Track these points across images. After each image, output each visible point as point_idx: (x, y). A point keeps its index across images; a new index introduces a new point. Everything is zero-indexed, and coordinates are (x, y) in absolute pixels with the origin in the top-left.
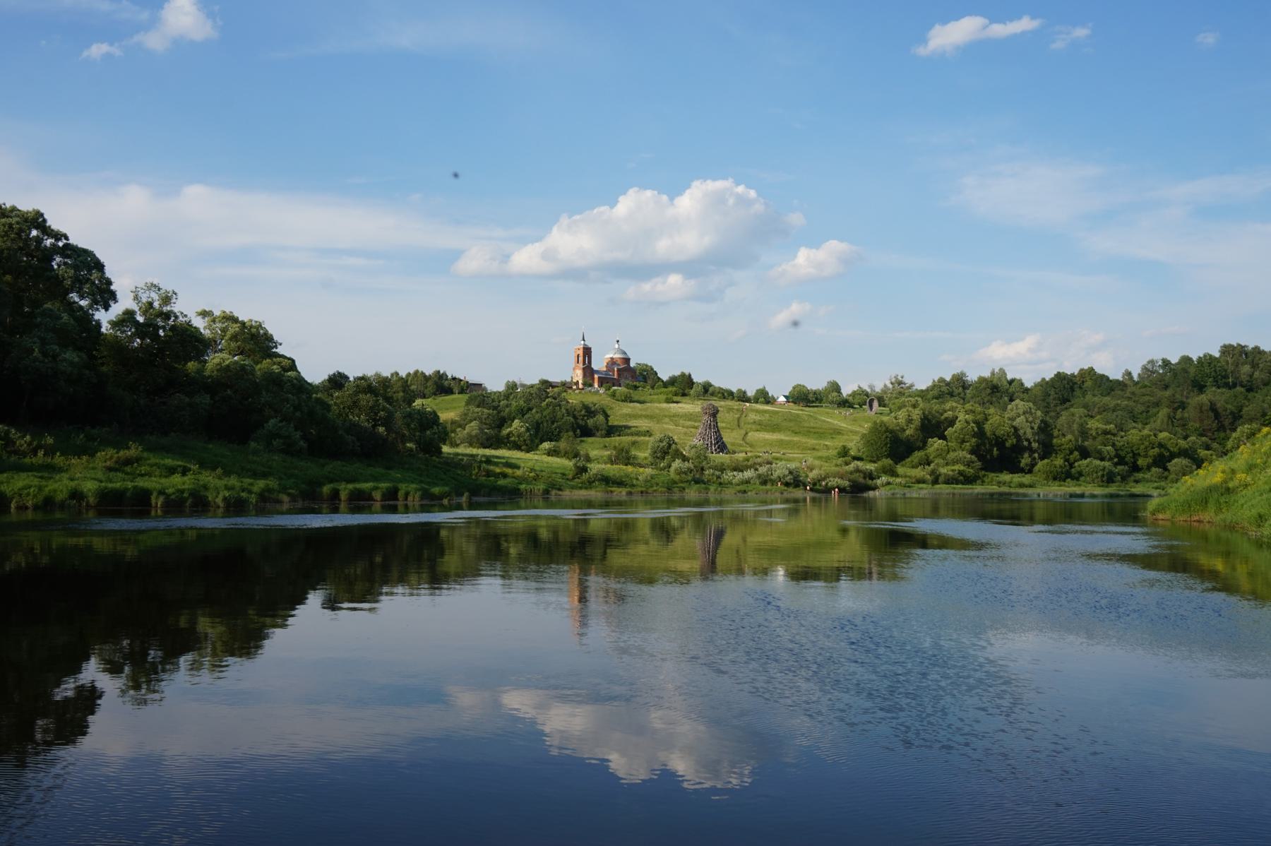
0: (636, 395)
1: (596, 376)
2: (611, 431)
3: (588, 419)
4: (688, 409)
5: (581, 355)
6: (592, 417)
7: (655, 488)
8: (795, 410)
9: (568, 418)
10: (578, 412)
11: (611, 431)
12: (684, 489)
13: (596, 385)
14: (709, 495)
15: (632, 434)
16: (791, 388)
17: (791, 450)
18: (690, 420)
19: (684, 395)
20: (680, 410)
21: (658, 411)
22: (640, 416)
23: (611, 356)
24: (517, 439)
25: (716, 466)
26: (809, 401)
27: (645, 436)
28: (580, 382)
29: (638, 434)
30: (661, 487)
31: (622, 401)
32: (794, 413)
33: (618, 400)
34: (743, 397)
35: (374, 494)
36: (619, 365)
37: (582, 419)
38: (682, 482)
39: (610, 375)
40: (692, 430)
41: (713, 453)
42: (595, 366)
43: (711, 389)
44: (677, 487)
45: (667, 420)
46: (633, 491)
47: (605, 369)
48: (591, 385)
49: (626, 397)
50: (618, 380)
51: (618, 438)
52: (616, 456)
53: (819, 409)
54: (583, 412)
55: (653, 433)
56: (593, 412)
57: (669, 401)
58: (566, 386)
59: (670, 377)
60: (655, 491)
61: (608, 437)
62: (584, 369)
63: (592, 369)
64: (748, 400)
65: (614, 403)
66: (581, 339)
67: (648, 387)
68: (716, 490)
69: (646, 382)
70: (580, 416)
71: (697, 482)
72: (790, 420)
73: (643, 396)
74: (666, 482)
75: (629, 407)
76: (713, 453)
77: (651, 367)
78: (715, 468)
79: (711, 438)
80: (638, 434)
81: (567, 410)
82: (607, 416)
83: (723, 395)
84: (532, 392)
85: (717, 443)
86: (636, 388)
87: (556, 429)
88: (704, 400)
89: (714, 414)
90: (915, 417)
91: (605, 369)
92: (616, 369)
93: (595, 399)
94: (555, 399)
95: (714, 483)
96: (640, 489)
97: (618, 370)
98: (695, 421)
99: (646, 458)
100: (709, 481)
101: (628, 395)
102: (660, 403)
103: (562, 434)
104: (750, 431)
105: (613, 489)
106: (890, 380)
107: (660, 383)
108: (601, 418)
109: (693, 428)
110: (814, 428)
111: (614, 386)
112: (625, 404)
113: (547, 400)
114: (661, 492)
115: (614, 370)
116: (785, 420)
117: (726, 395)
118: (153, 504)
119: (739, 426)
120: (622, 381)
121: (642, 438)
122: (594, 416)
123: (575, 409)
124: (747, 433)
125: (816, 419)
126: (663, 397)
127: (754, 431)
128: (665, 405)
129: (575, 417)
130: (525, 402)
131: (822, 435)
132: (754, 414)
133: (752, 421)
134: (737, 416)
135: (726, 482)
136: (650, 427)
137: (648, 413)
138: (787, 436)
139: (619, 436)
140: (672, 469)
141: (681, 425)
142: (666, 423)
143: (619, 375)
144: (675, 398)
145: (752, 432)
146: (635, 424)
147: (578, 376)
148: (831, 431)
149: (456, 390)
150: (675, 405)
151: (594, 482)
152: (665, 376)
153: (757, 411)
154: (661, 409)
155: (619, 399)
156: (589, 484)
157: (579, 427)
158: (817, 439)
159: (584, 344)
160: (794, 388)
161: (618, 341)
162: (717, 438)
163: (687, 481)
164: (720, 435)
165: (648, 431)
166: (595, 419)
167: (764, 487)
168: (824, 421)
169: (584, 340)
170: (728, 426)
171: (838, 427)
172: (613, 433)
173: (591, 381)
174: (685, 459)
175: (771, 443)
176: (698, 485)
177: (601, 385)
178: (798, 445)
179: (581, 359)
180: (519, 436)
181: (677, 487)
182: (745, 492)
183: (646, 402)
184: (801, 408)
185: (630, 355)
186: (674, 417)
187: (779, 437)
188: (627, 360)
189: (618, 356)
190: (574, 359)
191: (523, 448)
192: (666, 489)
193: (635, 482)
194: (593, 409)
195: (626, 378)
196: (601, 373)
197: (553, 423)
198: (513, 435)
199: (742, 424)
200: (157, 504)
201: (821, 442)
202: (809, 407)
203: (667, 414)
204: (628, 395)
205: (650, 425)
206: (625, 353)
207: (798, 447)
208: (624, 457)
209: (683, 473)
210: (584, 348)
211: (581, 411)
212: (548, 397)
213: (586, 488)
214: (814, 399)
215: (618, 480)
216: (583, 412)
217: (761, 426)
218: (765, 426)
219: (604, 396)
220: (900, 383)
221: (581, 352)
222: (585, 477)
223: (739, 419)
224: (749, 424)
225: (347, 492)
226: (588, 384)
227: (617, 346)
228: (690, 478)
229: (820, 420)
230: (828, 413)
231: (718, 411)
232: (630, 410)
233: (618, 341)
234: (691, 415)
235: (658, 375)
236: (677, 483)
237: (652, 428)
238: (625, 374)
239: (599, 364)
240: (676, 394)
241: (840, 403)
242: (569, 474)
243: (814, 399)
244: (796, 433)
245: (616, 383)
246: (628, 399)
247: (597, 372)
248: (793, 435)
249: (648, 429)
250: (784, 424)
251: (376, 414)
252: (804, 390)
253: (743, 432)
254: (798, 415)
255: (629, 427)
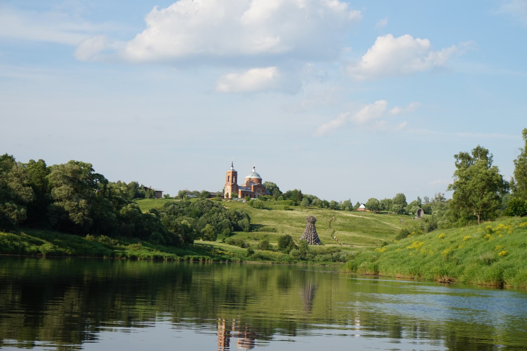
0: (266, 204)
1: (240, 190)
2: (252, 228)
3: (238, 220)
4: (298, 214)
5: (231, 176)
6: (240, 219)
7: (283, 262)
8: (370, 216)
9: (226, 219)
10: (232, 216)
11: (252, 228)
12: (296, 262)
13: (240, 196)
14: (308, 265)
15: (264, 230)
16: (368, 201)
17: (359, 243)
18: (299, 222)
19: (296, 205)
20: (294, 215)
21: (280, 216)
22: (269, 219)
23: (249, 177)
24: (208, 235)
25: (312, 252)
26: (379, 210)
27: (272, 232)
28: (230, 194)
29: (268, 230)
30: (286, 261)
31: (257, 208)
32: (366, 219)
33: (255, 208)
34: (335, 207)
35: (199, 259)
36: (254, 183)
37: (235, 220)
38: (296, 259)
39: (249, 190)
40: (301, 228)
41: (312, 244)
42: (239, 183)
43: (314, 201)
44: (293, 262)
45: (285, 221)
46: (274, 262)
47: (245, 186)
48: (237, 197)
49: (260, 205)
50: (254, 193)
51: (256, 233)
52: (261, 245)
53: (386, 215)
54: (235, 216)
55: (277, 230)
56: (241, 216)
57: (286, 209)
58: (221, 196)
59: (287, 192)
60: (283, 263)
61: (251, 232)
62: (232, 185)
63: (237, 185)
64: (338, 209)
65: (252, 209)
66: (231, 166)
67: (274, 199)
68: (311, 263)
69: (272, 195)
70: (233, 218)
71: (302, 259)
72: (363, 224)
73: (270, 205)
74: (288, 259)
75: (262, 212)
76: (312, 244)
77: (275, 184)
78: (312, 253)
79: (311, 235)
80: (268, 230)
81: (225, 214)
82: (249, 219)
83: (322, 205)
84: (204, 203)
85: (315, 238)
86: (266, 199)
87: (219, 227)
88: (309, 208)
89: (314, 221)
90: (425, 228)
91: (245, 186)
92: (252, 186)
93: (240, 206)
94: (217, 207)
95: (310, 260)
96: (277, 262)
97: (254, 187)
98: (303, 223)
99: (276, 247)
100: (308, 259)
101: (261, 205)
102: (281, 210)
103: (223, 229)
104: (336, 231)
105: (265, 261)
106: (435, 196)
107: (281, 197)
108: (245, 220)
109: (301, 227)
110: (377, 229)
111: (251, 198)
112: (259, 210)
113: (213, 208)
114: (286, 263)
115: (251, 187)
116: (360, 223)
117: (325, 205)
118: (164, 259)
119: (330, 227)
120: (257, 194)
121: (271, 233)
122: (242, 218)
123: (230, 214)
124: (334, 232)
125: (380, 223)
126: (283, 206)
127: (338, 230)
128: (284, 212)
129: (230, 219)
130: (199, 209)
131: (380, 234)
132: (340, 219)
133: (338, 224)
134: (329, 220)
135: (316, 260)
136: (275, 226)
137: (274, 216)
138: (359, 234)
139: (257, 231)
140: (291, 253)
141: (294, 225)
142: (285, 224)
143: (254, 190)
144: (291, 207)
145: (338, 231)
146: (265, 224)
147: (228, 190)
148: (387, 232)
149: (147, 195)
150: (291, 211)
151: (256, 258)
152: (284, 192)
153: (342, 217)
154: (283, 214)
155: (256, 206)
156: (255, 259)
157: (233, 225)
158: (377, 236)
159: (233, 170)
160: (369, 200)
161: (254, 168)
162: (314, 236)
163: (298, 259)
164: (317, 234)
165: (274, 229)
166: (242, 220)
167: (334, 263)
168: (385, 225)
169: (232, 166)
170: (323, 226)
171: (393, 229)
172: (253, 230)
173: (236, 194)
174: (297, 248)
175: (348, 239)
176: (302, 261)
177: (243, 196)
178: (364, 240)
179: (230, 179)
180: (209, 233)
181: (293, 262)
182: (324, 265)
183: (272, 209)
184: (373, 214)
185: (262, 177)
186: (290, 220)
187: (353, 235)
188: (260, 180)
189: (254, 177)
190: (225, 179)
191: (211, 239)
192: (288, 262)
193: (274, 259)
194: (241, 214)
195: (259, 192)
196: (243, 189)
197: (217, 222)
198: (206, 232)
199: (332, 226)
200: (147, 259)
201: (379, 239)
202: (379, 213)
203: (285, 217)
204: (261, 205)
205: (274, 225)
206: (259, 175)
207: (364, 242)
208: (266, 246)
209: (296, 255)
210: (233, 172)
211: (234, 215)
212: (213, 206)
213: (254, 260)
214: (382, 208)
215: (267, 257)
216: (235, 216)
217: (345, 227)
218: (346, 227)
219: (246, 204)
220: (442, 198)
221: (230, 175)
222: (253, 255)
223: (330, 222)
224: (336, 225)
225: (192, 258)
226: (234, 196)
227: (253, 171)
228: (299, 258)
229: (383, 224)
230: (389, 218)
231: (316, 220)
232: (262, 214)
233: (254, 168)
234: (301, 218)
235: (280, 190)
236: (293, 260)
237: (277, 227)
238: (259, 189)
239: (242, 182)
240: (291, 204)
241: (399, 212)
242: (246, 254)
243: (382, 208)
244: (365, 232)
245: (252, 195)
246: (261, 207)
247: (241, 187)
248: (363, 233)
249: (274, 227)
250: (360, 226)
251: (177, 229)
252: (376, 202)
253: (331, 231)
254: (368, 220)
255: (261, 226)
